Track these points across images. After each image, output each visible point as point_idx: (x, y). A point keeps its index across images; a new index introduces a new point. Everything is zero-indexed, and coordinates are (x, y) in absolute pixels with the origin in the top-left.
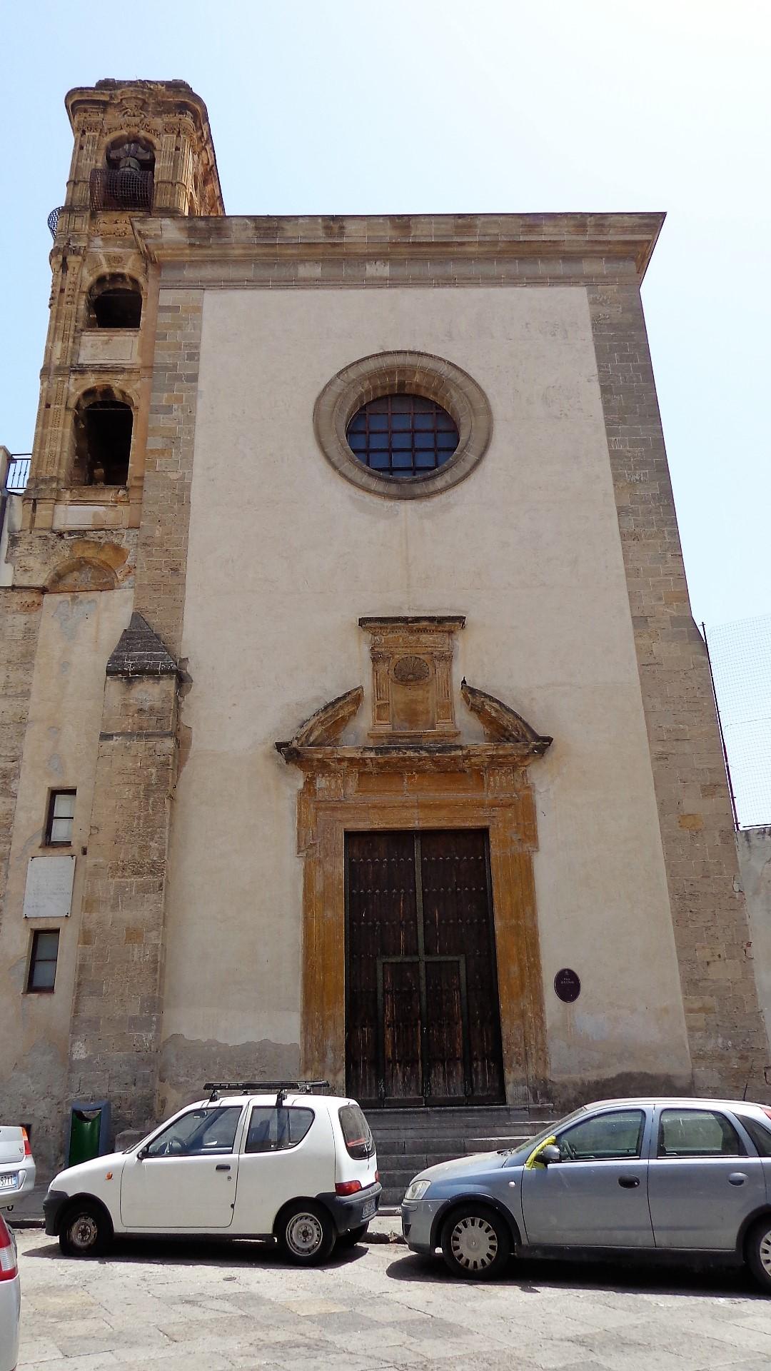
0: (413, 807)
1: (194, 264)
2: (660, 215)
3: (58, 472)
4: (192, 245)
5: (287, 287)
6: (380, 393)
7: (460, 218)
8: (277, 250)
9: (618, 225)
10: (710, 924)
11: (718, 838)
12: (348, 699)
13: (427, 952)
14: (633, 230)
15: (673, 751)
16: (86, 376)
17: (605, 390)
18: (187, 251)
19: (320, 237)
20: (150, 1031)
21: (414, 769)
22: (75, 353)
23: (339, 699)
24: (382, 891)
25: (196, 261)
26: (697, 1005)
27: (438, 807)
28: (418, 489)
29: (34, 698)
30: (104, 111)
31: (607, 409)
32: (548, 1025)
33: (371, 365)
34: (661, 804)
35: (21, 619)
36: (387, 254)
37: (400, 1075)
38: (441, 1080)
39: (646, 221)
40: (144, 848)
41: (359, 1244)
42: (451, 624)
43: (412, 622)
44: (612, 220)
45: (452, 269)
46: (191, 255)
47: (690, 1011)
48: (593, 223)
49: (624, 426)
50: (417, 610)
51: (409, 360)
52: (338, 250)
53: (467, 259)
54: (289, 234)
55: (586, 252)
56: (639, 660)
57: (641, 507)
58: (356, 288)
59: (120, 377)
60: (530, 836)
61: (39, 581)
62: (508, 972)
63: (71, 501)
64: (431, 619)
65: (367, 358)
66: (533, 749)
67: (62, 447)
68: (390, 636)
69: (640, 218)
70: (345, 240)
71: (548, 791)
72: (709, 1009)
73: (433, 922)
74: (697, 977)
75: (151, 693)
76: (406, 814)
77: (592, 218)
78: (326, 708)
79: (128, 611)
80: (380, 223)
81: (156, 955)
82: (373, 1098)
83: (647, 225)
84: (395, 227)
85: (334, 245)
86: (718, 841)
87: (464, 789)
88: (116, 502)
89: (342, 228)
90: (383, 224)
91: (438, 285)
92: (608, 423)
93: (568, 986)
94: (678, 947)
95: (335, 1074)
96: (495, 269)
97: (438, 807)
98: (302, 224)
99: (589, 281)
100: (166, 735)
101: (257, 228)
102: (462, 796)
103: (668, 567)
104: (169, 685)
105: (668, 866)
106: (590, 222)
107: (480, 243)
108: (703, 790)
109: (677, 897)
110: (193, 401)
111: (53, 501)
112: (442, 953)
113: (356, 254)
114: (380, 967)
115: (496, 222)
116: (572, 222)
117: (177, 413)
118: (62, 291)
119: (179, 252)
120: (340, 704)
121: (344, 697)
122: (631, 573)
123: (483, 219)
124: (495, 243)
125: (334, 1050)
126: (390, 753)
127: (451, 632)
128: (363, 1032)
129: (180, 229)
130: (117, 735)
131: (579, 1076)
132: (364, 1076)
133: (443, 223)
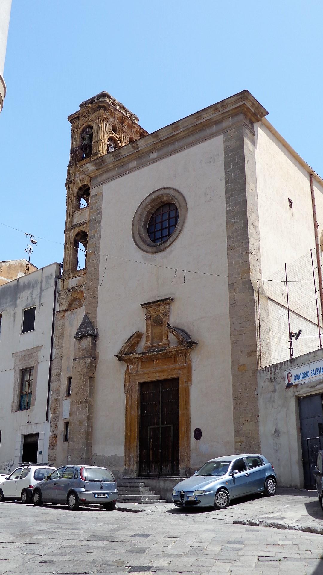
0: (156, 372)
1: (101, 175)
2: (244, 91)
3: (69, 267)
4: (97, 169)
5: (126, 174)
6: (157, 207)
7: (173, 125)
8: (122, 160)
9: (230, 103)
10: (246, 408)
11: (251, 373)
12: (134, 336)
13: (163, 424)
14: (236, 102)
15: (239, 339)
16: (76, 229)
17: (227, 182)
18: (97, 172)
19: (132, 151)
20: (84, 452)
21: (157, 358)
22: (73, 221)
23: (131, 337)
24: (151, 403)
25: (101, 174)
26: (238, 440)
27: (163, 371)
28: (162, 247)
29: (64, 348)
30: (79, 120)
31: (227, 192)
32: (191, 448)
33: (150, 199)
34: (233, 362)
35: (61, 322)
36: (154, 148)
37: (154, 466)
38: (165, 468)
39: (239, 97)
40: (83, 395)
41: (80, 507)
42: (168, 301)
43: (155, 303)
44: (227, 101)
45: (177, 145)
46: (99, 172)
47: (236, 442)
48: (220, 106)
49: (232, 198)
50: (160, 297)
51: (161, 192)
52: (140, 153)
53: (181, 138)
54: (123, 154)
55: (223, 118)
56: (230, 303)
57: (235, 234)
58: (146, 166)
59: (84, 226)
60: (189, 379)
61: (64, 308)
62: (182, 429)
63: (73, 277)
64: (160, 301)
65: (148, 196)
66: (187, 347)
67: (70, 258)
68: (151, 309)
69: (237, 96)
70: (140, 149)
71: (196, 361)
72: (242, 442)
73: (165, 413)
74: (239, 429)
75: (86, 343)
76: (155, 375)
77: (219, 104)
78: (127, 341)
79: (83, 314)
80: (148, 138)
81: (86, 429)
82: (146, 473)
83: (241, 98)
84: (154, 137)
85: (137, 152)
86: (251, 375)
87: (171, 364)
88: (83, 274)
89: (137, 145)
90: (149, 138)
91: (172, 154)
92: (227, 198)
93: (198, 434)
94: (234, 418)
95: (133, 466)
96: (192, 139)
97: (163, 371)
98: (125, 149)
99: (223, 131)
100: (88, 357)
101: (113, 156)
102: (170, 366)
103: (243, 259)
104: (89, 339)
105: (233, 386)
106: (219, 106)
107: (184, 131)
108: (248, 354)
109: (235, 398)
110: (100, 231)
111: (68, 279)
112: (167, 424)
113: (146, 152)
114: (149, 430)
115: (186, 121)
116: (212, 109)
117: (96, 237)
118: (69, 198)
119: (95, 173)
120: (132, 339)
121: (132, 336)
122: (230, 265)
123: (181, 122)
124: (188, 129)
125: (133, 458)
126: (146, 354)
127: (169, 304)
128: (144, 452)
129: (93, 165)
130: (77, 359)
131: (199, 466)
132: (144, 466)
133: (168, 129)
